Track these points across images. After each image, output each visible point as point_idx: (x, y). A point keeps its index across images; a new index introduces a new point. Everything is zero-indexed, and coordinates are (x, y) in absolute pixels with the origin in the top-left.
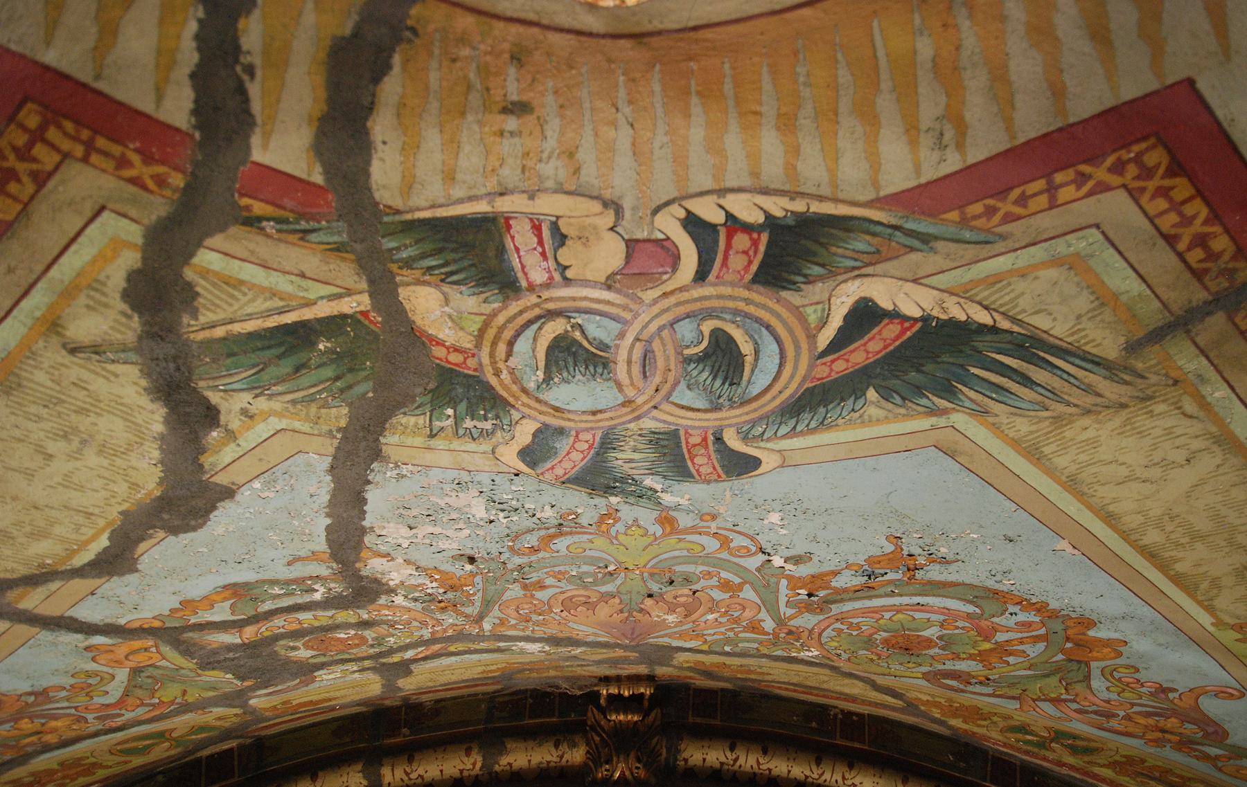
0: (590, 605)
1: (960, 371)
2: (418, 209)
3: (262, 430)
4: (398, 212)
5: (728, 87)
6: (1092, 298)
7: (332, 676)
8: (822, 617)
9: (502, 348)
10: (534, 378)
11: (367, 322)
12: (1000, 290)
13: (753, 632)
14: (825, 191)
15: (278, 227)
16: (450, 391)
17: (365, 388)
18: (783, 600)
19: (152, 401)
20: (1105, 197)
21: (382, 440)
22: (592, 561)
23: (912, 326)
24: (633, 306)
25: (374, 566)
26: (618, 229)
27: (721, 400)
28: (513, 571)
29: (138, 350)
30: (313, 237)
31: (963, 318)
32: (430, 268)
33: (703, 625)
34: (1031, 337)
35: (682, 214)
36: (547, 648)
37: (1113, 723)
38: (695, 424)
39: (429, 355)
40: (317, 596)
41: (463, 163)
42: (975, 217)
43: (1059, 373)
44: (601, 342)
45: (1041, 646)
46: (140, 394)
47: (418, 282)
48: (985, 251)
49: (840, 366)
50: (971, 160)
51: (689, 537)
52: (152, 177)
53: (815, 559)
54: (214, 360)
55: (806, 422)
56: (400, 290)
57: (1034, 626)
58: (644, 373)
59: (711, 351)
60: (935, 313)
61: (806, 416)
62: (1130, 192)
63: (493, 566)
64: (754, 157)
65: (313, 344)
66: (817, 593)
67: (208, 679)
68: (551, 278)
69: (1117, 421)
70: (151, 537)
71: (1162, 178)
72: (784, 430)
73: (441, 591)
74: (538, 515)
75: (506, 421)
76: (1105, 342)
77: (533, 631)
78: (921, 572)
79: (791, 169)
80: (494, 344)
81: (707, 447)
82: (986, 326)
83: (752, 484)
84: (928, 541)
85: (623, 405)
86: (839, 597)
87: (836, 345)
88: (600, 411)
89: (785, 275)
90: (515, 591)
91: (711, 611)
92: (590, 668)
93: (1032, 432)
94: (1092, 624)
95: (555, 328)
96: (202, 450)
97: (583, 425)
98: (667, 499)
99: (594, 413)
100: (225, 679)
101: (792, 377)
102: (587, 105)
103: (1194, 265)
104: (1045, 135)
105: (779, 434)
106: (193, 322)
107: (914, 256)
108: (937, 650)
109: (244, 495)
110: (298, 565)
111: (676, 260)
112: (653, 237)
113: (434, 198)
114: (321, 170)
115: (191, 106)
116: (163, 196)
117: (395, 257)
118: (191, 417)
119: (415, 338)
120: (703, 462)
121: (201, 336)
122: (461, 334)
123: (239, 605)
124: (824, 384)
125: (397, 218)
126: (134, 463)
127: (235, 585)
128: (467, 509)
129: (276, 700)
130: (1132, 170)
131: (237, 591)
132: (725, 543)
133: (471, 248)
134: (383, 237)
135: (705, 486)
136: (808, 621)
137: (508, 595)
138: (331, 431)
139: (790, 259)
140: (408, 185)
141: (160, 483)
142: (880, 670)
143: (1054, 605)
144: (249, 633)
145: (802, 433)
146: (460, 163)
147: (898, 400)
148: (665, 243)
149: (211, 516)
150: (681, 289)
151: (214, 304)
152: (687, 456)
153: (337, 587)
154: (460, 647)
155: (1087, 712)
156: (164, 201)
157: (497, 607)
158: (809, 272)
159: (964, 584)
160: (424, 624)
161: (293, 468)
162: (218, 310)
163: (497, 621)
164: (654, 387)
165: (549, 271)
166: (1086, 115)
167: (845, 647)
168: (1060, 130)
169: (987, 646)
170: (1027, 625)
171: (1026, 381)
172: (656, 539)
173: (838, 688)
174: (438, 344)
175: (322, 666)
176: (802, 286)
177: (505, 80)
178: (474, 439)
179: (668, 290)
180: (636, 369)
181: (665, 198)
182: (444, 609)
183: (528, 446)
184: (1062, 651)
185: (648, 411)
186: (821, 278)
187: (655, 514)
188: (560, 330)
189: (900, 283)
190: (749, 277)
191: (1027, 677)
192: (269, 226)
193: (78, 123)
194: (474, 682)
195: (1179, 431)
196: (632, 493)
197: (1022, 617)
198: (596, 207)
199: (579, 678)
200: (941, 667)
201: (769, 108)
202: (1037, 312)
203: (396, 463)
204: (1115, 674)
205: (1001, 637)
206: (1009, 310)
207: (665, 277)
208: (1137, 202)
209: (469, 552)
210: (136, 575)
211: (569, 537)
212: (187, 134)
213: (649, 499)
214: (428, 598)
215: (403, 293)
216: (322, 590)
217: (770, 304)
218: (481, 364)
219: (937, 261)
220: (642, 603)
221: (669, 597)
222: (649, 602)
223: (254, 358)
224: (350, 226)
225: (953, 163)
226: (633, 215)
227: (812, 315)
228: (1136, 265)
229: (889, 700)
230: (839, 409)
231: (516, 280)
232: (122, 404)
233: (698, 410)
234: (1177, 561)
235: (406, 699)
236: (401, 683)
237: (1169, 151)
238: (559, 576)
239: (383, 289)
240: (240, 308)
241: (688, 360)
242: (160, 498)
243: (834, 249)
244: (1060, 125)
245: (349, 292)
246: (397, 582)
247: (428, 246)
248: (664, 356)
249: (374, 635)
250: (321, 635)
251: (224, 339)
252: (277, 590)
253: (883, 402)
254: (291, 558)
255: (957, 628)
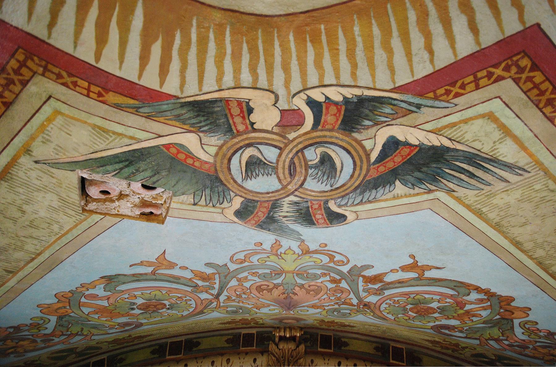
1: (439, 171)
8: (381, 297)
18: (361, 288)
20: (502, 83)
23: (415, 149)
26: (277, 105)
37: (527, 352)
42: (441, 95)
45: (489, 311)
49: (382, 169)
51: (315, 256)
62: (514, 80)
71: (529, 72)
85: (282, 189)
89: (353, 125)
101: (359, 175)
103: (548, 115)
105: (355, 203)
120: (319, 216)
130: (514, 70)
132: (332, 258)
147: (410, 185)
155: (513, 346)
169: (461, 312)
171: (472, 175)
172: (299, 256)
180: (287, 172)
193: (41, 59)
195: (548, 198)
202: (474, 141)
205: (468, 307)
206: (461, 140)
227: (368, 144)
234: (553, 265)
237: (531, 60)
243: (376, 112)
255: (447, 302)
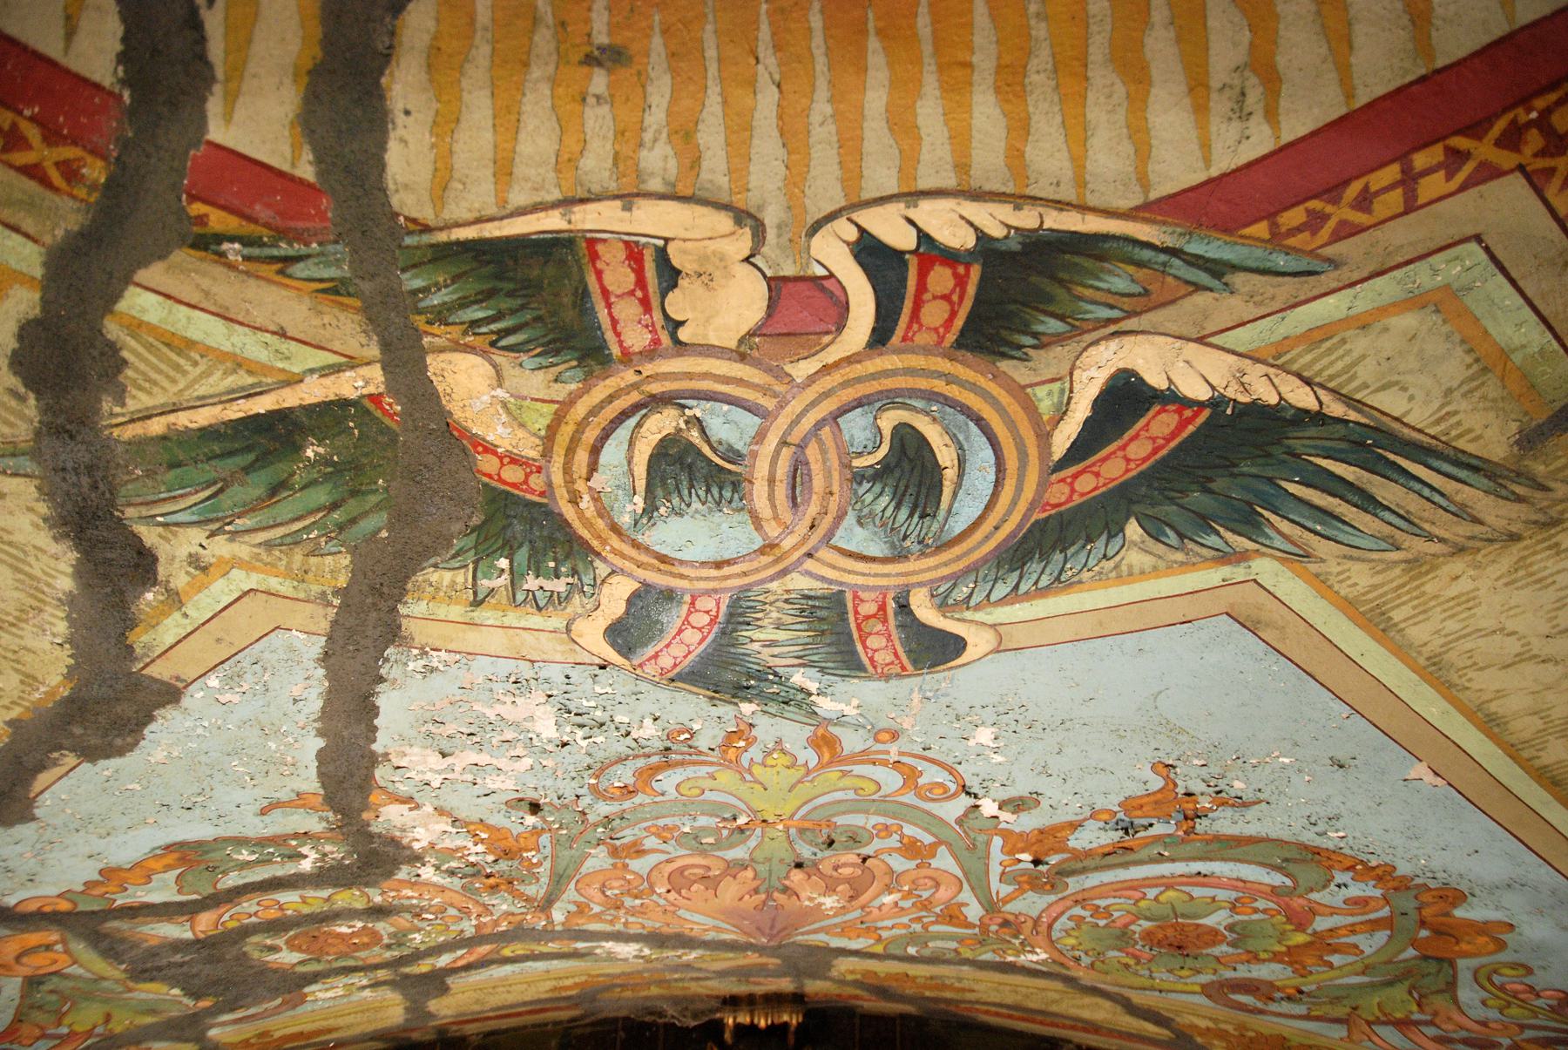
0: (710, 882)
2: (458, 225)
3: (221, 591)
4: (427, 229)
5: (923, 23)
6: (1469, 360)
7: (330, 994)
9: (582, 457)
10: (629, 508)
11: (378, 414)
12: (1330, 351)
13: (950, 923)
14: (1067, 193)
15: (246, 251)
16: (504, 528)
17: (376, 523)
18: (995, 870)
19: (55, 539)
21: (402, 610)
22: (714, 809)
23: (1196, 415)
24: (779, 388)
25: (390, 818)
26: (757, 260)
27: (908, 543)
28: (596, 825)
29: (35, 454)
30: (299, 269)
31: (1273, 399)
32: (475, 323)
33: (876, 911)
34: (1376, 429)
35: (852, 234)
36: (647, 951)
38: (868, 582)
39: (472, 469)
40: (306, 866)
41: (525, 147)
42: (1293, 232)
43: (1418, 486)
44: (731, 448)
45: (1381, 936)
46: (37, 526)
47: (458, 347)
48: (1308, 286)
49: (1086, 484)
50: (1287, 137)
51: (858, 769)
52: (57, 164)
53: (1045, 803)
54: (150, 474)
55: (1035, 577)
56: (429, 360)
57: (1373, 904)
58: (794, 498)
59: (893, 461)
60: (1230, 393)
61: (1034, 567)
62: (1528, 177)
63: (567, 817)
64: (960, 140)
65: (298, 449)
66: (1048, 860)
67: (143, 996)
68: (656, 342)
69: (1506, 562)
70: (55, 763)
72: (1001, 590)
73: (490, 858)
74: (634, 734)
75: (587, 579)
76: (1489, 433)
77: (626, 924)
78: (1205, 822)
79: (1016, 158)
80: (570, 451)
81: (885, 621)
82: (1307, 412)
83: (952, 681)
84: (1215, 770)
85: (762, 551)
86: (1079, 865)
87: (1081, 449)
88: (728, 562)
89: (1004, 333)
90: (599, 859)
91: (889, 889)
92: (709, 983)
93: (1375, 587)
94: (1459, 897)
95: (662, 423)
96: (130, 623)
97: (702, 585)
98: (826, 706)
99: (718, 565)
100: (170, 997)
101: (1014, 503)
102: (711, 53)
104: (1399, 90)
105: (993, 598)
106: (117, 410)
107: (1201, 299)
108: (1224, 948)
109: (195, 698)
110: (277, 813)
111: (841, 310)
112: (809, 273)
113: (476, 208)
114: (311, 157)
115: (119, 47)
116: (74, 197)
117: (422, 305)
118: (116, 568)
119: (454, 440)
120: (880, 645)
121: (130, 432)
122: (521, 433)
123: (189, 877)
124: (1061, 514)
125: (426, 239)
126: (30, 642)
127: (182, 844)
128: (528, 725)
129: (248, 1031)
130: (1534, 140)
131: (186, 855)
132: (910, 777)
133: (537, 291)
134: (404, 270)
135: (881, 684)
136: (1031, 904)
137: (589, 865)
138: (324, 593)
139: (1013, 307)
140: (443, 182)
141: (68, 676)
142: (1137, 981)
143: (1403, 869)
144: (206, 922)
145: (1028, 596)
146: (520, 148)
147: (1173, 538)
148: (825, 283)
149: (146, 731)
150: (850, 360)
151: (149, 380)
152: (856, 635)
153: (336, 852)
154: (518, 949)
155: (1450, 1041)
156: (76, 205)
157: (572, 885)
158: (1040, 328)
159: (1267, 840)
160: (465, 912)
161: (267, 655)
162: (155, 390)
163: (573, 908)
164: (807, 522)
165: (654, 332)
166: (1462, 53)
167: (1087, 945)
168: (1422, 79)
169: (1300, 938)
170: (1361, 903)
171: (1368, 503)
172: (808, 772)
173: (1074, 1012)
174: (486, 450)
175: (315, 978)
176: (1031, 352)
177: (590, 9)
178: (539, 609)
179: (830, 360)
180: (782, 491)
181: (829, 208)
182: (494, 889)
183: (619, 621)
184: (1414, 943)
185: (799, 562)
186: (1060, 339)
187: (808, 731)
188: (669, 429)
189: (1179, 343)
190: (951, 337)
191: (1361, 986)
192: (233, 250)
194: (539, 1006)
196: (774, 697)
197: (1356, 890)
198: (724, 222)
199: (693, 999)
200: (1229, 974)
201: (984, 59)
202: (1383, 388)
203: (422, 648)
204: (1496, 979)
205: (1321, 924)
207: (826, 339)
208: (1539, 192)
209: (531, 795)
210: (33, 825)
211: (679, 770)
212: (111, 93)
213: (799, 706)
214: (470, 870)
215: (434, 363)
216: (313, 855)
217: (982, 382)
218: (550, 484)
219: (1235, 306)
220: (787, 877)
221: (825, 867)
222: (797, 876)
223: (210, 470)
224: (354, 251)
225: (1260, 142)
226: (779, 236)
227: (1045, 398)
228: (1537, 302)
229: (1150, 1028)
230: (1084, 554)
231: (603, 345)
232: (10, 544)
233: (873, 559)
235: (442, 1031)
236: (433, 1005)
238: (664, 834)
239: (404, 360)
240: (187, 387)
241: (859, 477)
242: (69, 701)
243: (1079, 290)
244: (1423, 71)
245: (352, 363)
246: (424, 843)
247: (471, 287)
248: (823, 472)
249: (392, 930)
250: (312, 929)
251: (164, 438)
252: (245, 855)
253: (1150, 542)
254: (265, 803)
255: (1256, 911)
